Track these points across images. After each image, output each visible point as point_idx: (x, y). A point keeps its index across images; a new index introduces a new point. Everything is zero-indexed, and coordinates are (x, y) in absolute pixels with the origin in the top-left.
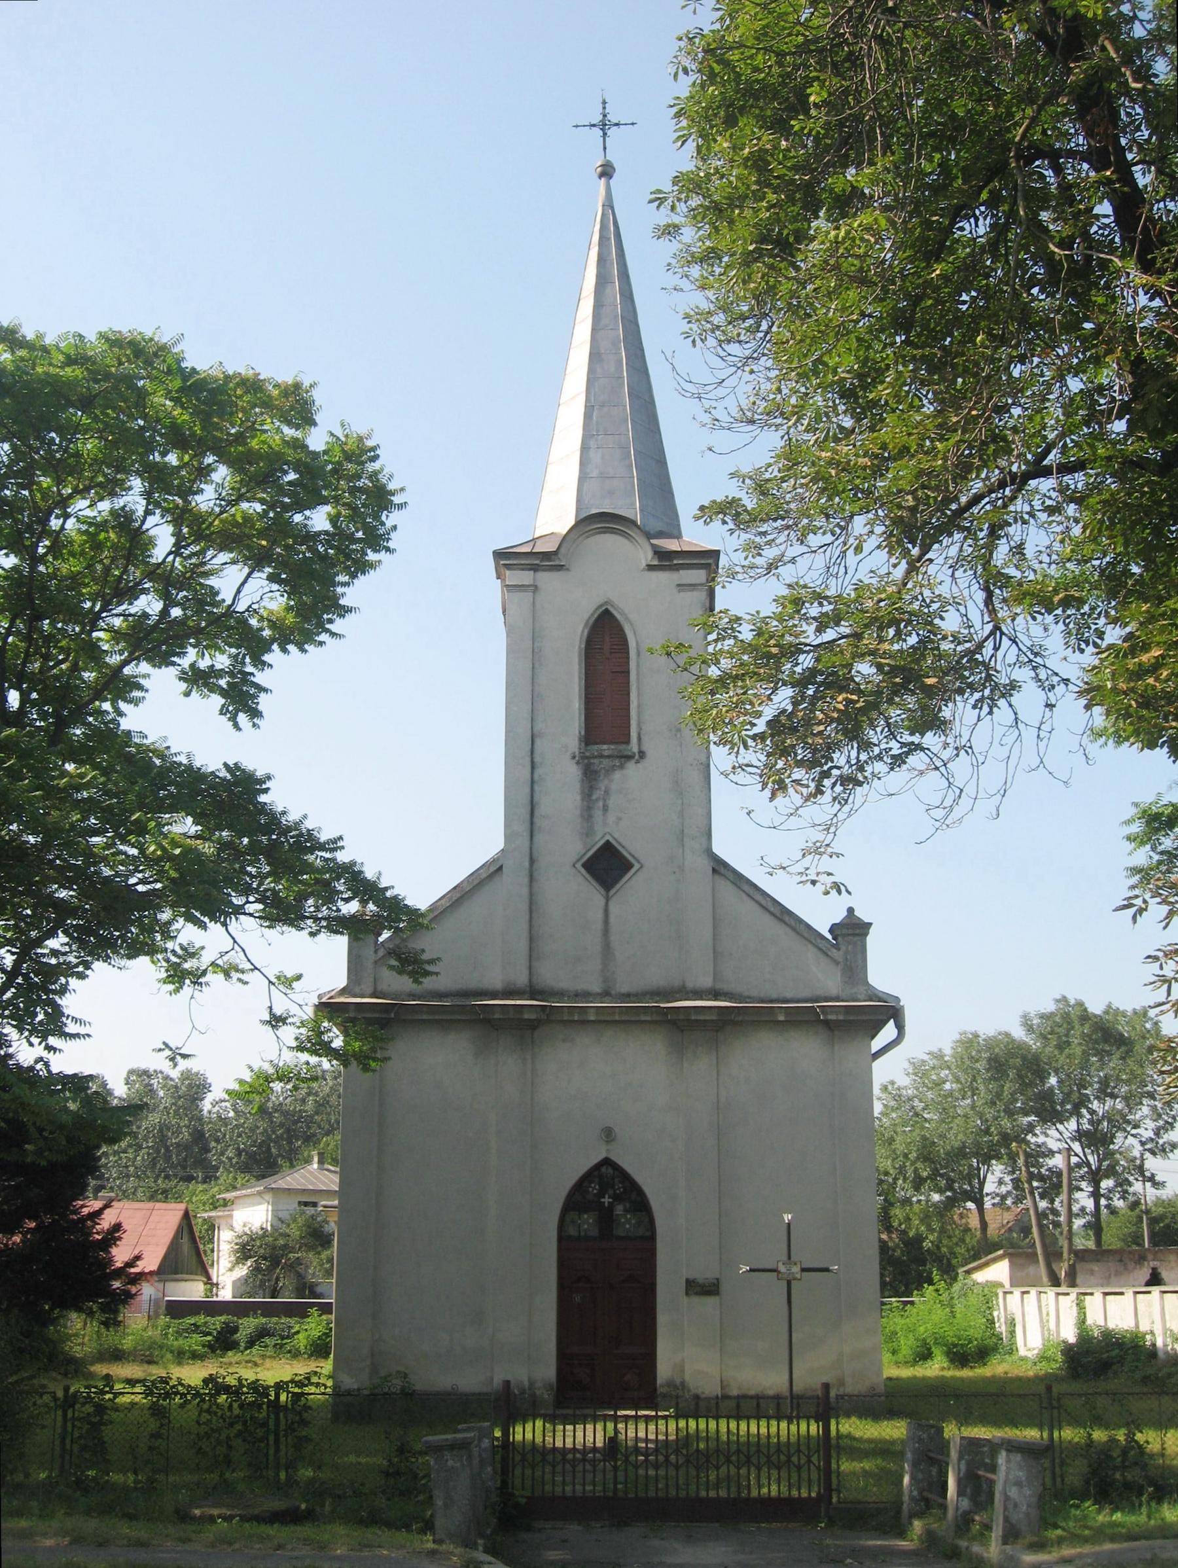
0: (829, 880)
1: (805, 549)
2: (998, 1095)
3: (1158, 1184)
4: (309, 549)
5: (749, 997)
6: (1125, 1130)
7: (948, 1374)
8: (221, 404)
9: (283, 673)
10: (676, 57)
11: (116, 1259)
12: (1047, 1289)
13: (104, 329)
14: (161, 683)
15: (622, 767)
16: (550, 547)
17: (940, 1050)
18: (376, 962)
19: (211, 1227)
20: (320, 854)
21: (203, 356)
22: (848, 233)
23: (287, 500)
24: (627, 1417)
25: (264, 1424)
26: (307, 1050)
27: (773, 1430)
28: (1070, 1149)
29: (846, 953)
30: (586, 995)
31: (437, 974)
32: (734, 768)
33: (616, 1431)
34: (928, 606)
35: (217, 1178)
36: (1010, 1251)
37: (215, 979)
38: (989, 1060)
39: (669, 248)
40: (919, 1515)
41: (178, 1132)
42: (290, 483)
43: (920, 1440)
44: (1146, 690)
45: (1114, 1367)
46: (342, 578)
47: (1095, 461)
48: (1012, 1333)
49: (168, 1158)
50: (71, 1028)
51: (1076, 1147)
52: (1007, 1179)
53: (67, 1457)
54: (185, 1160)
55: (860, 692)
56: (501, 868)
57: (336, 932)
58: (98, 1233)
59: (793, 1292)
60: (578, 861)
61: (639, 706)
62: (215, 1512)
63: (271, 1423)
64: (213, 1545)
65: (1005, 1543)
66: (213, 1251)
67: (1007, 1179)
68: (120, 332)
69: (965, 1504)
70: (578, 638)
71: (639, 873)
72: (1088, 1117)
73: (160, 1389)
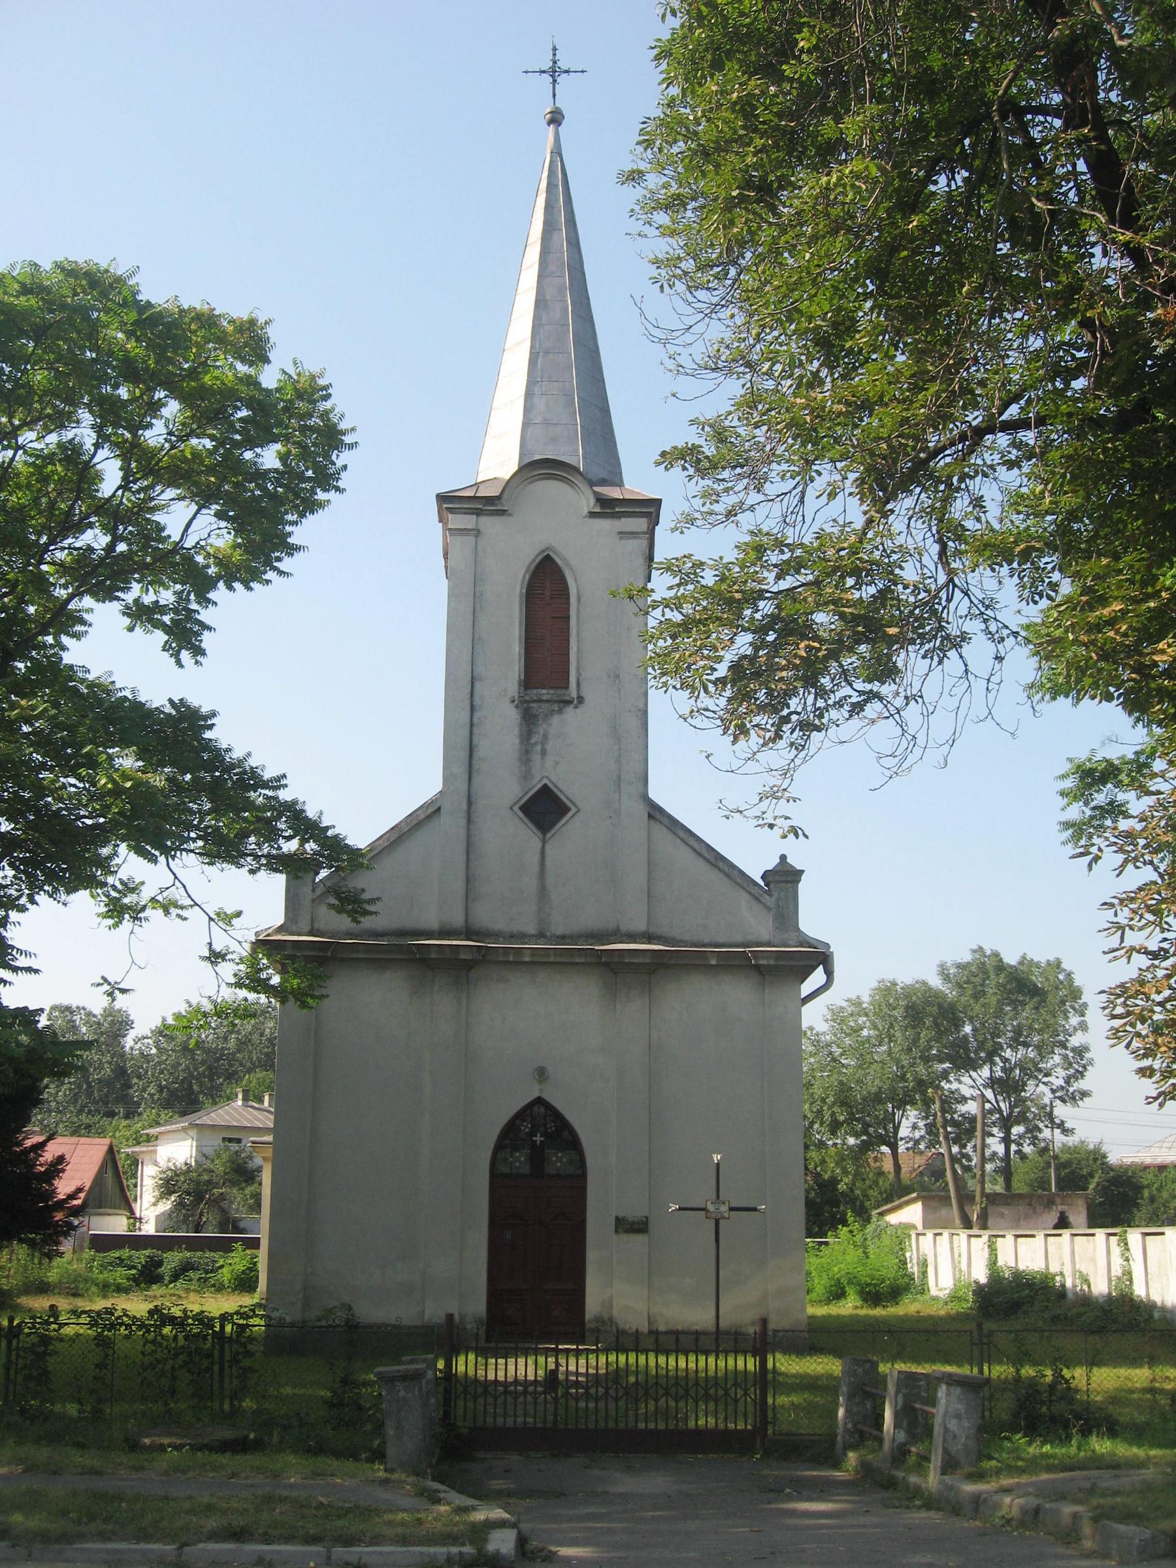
2: (915, 1042)
4: (258, 486)
5: (682, 941)
6: (1036, 1078)
7: (863, 1312)
8: (175, 338)
9: (228, 610)
11: (58, 1191)
12: (960, 1231)
13: (60, 258)
14: (104, 618)
15: (560, 711)
16: (493, 492)
17: (858, 997)
18: (313, 901)
19: (135, 1162)
20: (263, 791)
21: (157, 289)
22: (840, 179)
23: (238, 437)
24: (567, 1351)
25: (209, 1355)
26: (247, 987)
27: (702, 1364)
28: (983, 1095)
29: (779, 899)
30: (522, 937)
31: (376, 913)
32: (692, 711)
33: (557, 1364)
34: (889, 557)
35: (140, 1114)
36: (924, 1194)
37: (154, 915)
38: (907, 1007)
39: (633, 194)
40: (853, 1447)
41: (101, 1067)
42: (241, 420)
44: (1104, 644)
45: (1024, 1307)
47: (1055, 417)
48: (924, 1274)
49: (90, 1094)
50: (22, 962)
51: (989, 1094)
52: (921, 1124)
53: (11, 1387)
54: (106, 1096)
55: (821, 641)
56: (439, 808)
57: (276, 870)
58: (41, 1165)
60: (515, 804)
61: (578, 651)
62: (166, 1441)
63: (216, 1353)
64: (166, 1473)
65: (943, 1474)
66: (135, 1186)
67: (921, 1124)
68: (76, 262)
69: (902, 1436)
70: (519, 582)
71: (576, 818)
73: (105, 1320)
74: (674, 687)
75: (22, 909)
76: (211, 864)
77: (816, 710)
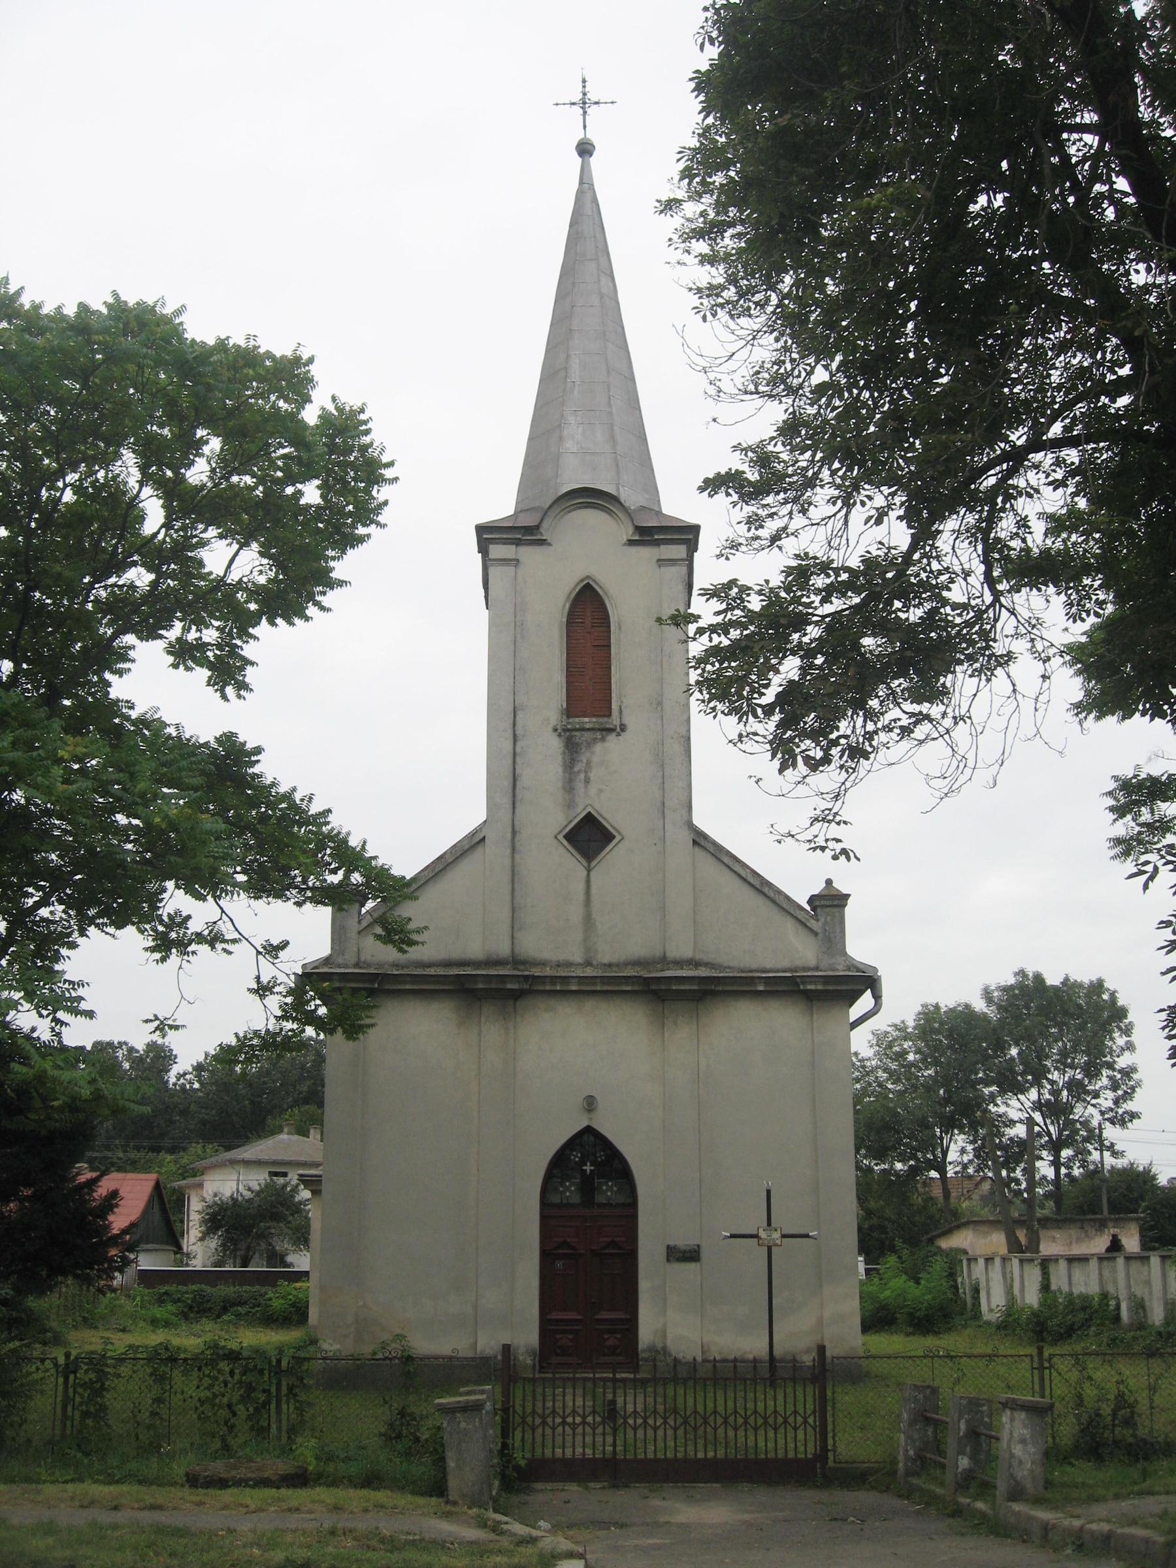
0: (838, 847)
1: (807, 522)
3: (1117, 1153)
5: (729, 967)
6: (1084, 1100)
10: (703, 27)
15: (603, 739)
17: (903, 1022)
21: (201, 329)
32: (740, 736)
39: (673, 223)
42: (284, 457)
43: (916, 1400)
46: (330, 553)
52: (970, 1148)
53: (68, 1423)
59: (774, 1257)
67: (970, 1148)
71: (620, 845)
72: (1049, 1087)
74: (723, 712)
75: (73, 946)
76: (257, 898)
77: (866, 733)
